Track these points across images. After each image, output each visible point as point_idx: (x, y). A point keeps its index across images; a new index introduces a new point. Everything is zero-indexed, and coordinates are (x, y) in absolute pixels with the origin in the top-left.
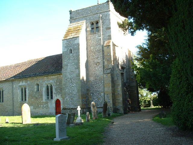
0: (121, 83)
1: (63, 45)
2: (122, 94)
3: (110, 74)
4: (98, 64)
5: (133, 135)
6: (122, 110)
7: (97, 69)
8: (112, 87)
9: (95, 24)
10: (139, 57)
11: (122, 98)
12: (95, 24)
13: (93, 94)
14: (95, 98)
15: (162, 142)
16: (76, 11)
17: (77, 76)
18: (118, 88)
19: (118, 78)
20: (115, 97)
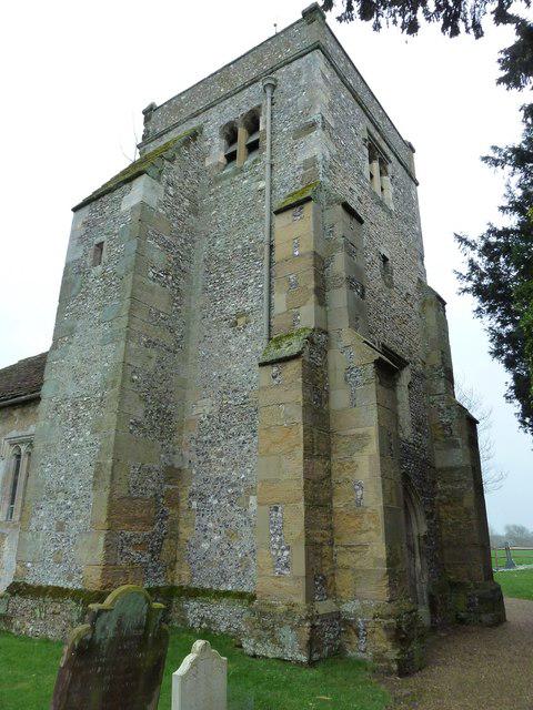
0: (373, 431)
1: (73, 231)
2: (386, 508)
3: (294, 369)
4: (241, 321)
5: (37, 611)
6: (373, 645)
7: (233, 348)
8: (310, 452)
9: (242, 132)
10: (503, 73)
11: (381, 537)
12: (242, 132)
13: (203, 498)
14: (211, 525)
15: (222, 520)
16: (169, 102)
17: (72, 331)
18: (354, 466)
19: (353, 397)
20: (331, 528)
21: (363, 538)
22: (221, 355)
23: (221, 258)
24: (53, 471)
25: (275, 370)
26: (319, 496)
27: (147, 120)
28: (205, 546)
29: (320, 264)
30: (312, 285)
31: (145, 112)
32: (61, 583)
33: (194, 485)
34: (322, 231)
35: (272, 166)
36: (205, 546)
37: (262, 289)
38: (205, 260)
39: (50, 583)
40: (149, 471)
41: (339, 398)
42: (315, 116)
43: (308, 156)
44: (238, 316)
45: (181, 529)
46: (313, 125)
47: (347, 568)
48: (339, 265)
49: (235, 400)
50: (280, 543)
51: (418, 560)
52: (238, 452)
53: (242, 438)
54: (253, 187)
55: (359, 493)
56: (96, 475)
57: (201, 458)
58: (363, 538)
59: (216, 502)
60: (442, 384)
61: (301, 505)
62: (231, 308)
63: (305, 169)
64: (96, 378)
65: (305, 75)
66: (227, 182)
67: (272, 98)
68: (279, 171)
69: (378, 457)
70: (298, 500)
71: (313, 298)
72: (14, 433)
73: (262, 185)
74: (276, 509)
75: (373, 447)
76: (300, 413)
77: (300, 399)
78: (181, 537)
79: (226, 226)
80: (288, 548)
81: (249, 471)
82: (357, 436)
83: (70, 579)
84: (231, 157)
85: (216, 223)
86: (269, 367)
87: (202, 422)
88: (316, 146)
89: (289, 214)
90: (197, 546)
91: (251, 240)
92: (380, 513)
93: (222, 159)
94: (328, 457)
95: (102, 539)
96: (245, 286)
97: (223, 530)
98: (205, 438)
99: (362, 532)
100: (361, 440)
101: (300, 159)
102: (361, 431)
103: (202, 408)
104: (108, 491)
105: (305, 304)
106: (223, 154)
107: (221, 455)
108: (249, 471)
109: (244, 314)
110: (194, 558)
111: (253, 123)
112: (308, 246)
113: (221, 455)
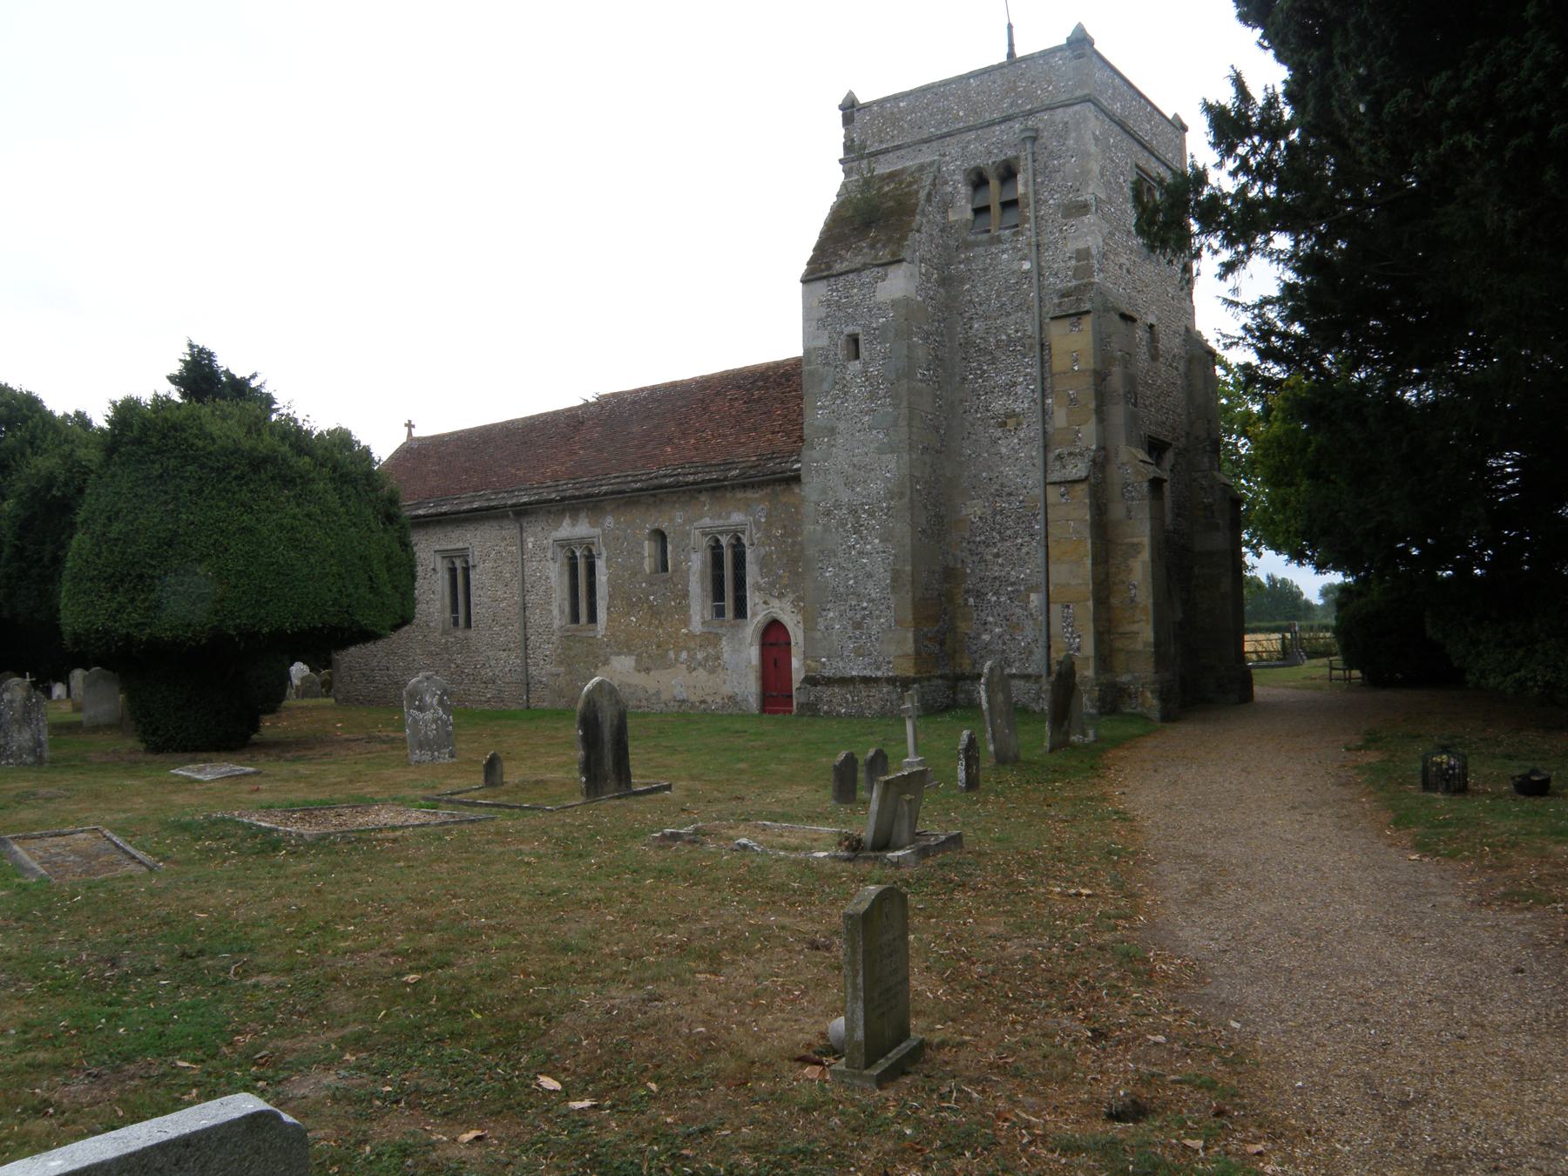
3: (1083, 490)
4: (1011, 423)
7: (1004, 450)
13: (979, 595)
21: (1135, 627)
22: (989, 455)
23: (982, 346)
24: (836, 575)
25: (1063, 489)
26: (1104, 590)
27: (848, 120)
28: (986, 637)
29: (1101, 377)
30: (1092, 405)
31: (841, 107)
32: (867, 673)
33: (969, 584)
34: (1102, 342)
35: (1038, 246)
36: (986, 637)
37: (1033, 391)
38: (961, 344)
39: (854, 673)
40: (933, 572)
41: (1117, 511)
42: (1087, 196)
43: (1081, 245)
44: (1008, 416)
45: (959, 624)
46: (1083, 208)
47: (1122, 650)
48: (1116, 380)
49: (1010, 504)
50: (1072, 633)
51: (416, 816)
52: (1015, 554)
53: (1020, 541)
54: (1015, 266)
55: (1133, 592)
56: (894, 580)
57: (976, 558)
58: (1135, 627)
59: (994, 599)
60: (1206, 460)
61: (1090, 603)
62: (998, 407)
63: (1078, 261)
64: (876, 487)
65: (1073, 135)
66: (981, 250)
67: (1033, 154)
68: (1048, 255)
69: (1150, 565)
70: (1088, 600)
71: (1093, 418)
72: (707, 521)
73: (1026, 266)
74: (1068, 607)
75: (1146, 555)
76: (1088, 530)
77: (1088, 517)
78: (959, 630)
79: (984, 307)
80: (1079, 636)
81: (1028, 571)
82: (1133, 545)
83: (878, 668)
84: (981, 211)
85: (970, 301)
86: (1058, 486)
87: (973, 523)
88: (1089, 234)
89: (1066, 323)
90: (978, 636)
91: (1017, 331)
92: (1150, 607)
93: (969, 215)
94: (1107, 562)
95: (910, 635)
96: (1015, 384)
97: (1004, 622)
98: (978, 539)
99: (1134, 622)
100: (1135, 549)
101: (1072, 246)
102: (1135, 540)
103: (974, 510)
104: (910, 594)
105: (1086, 422)
106: (969, 207)
107: (997, 555)
108: (1028, 571)
109: (1012, 415)
110: (974, 648)
111: (1008, 173)
112: (1088, 362)
113: (997, 555)
